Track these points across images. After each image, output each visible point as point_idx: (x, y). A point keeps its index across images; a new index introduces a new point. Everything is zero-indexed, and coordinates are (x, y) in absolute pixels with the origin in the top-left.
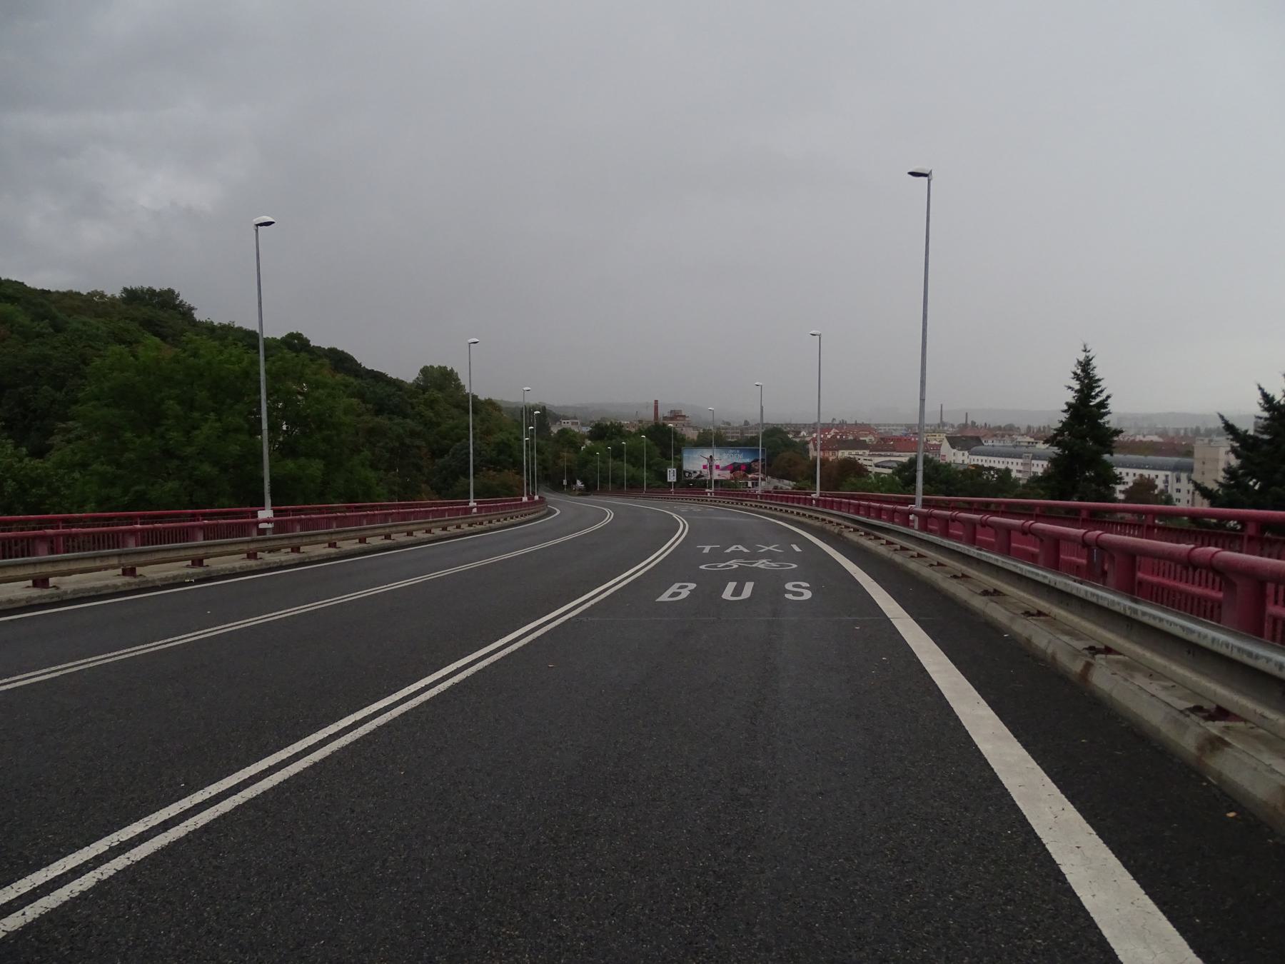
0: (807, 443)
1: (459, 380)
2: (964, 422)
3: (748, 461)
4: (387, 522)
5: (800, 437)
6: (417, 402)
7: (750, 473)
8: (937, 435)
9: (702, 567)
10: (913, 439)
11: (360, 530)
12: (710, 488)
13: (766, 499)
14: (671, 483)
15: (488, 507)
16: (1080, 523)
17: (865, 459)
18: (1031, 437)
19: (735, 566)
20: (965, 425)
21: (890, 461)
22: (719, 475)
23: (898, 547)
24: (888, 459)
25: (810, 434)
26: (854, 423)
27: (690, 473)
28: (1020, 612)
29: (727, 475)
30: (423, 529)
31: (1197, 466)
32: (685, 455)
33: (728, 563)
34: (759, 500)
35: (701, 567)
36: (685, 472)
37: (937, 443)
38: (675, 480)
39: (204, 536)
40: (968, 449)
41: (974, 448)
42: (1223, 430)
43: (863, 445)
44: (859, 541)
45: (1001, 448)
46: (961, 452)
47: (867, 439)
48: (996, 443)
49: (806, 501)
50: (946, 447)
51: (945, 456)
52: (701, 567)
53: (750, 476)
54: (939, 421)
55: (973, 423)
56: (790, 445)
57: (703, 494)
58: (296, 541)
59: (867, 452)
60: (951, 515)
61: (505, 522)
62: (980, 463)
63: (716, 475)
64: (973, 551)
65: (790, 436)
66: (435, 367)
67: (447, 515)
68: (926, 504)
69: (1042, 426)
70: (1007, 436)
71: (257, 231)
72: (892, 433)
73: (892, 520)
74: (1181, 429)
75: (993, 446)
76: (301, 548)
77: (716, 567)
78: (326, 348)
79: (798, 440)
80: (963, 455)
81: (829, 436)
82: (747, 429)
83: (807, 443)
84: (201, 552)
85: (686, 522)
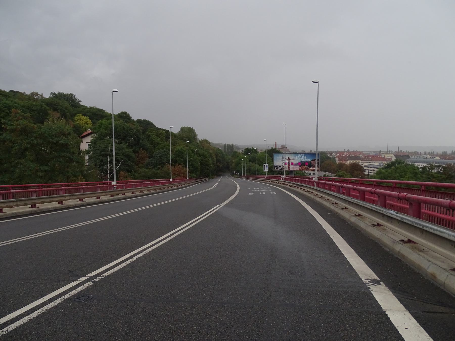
0: (335, 158)
1: (195, 132)
2: (398, 150)
5: (332, 156)
6: (152, 134)
7: (310, 167)
8: (389, 154)
10: (379, 156)
11: (148, 188)
12: (283, 175)
13: (295, 182)
14: (265, 172)
16: (374, 186)
21: (371, 165)
22: (293, 168)
23: (311, 192)
24: (370, 164)
25: (336, 154)
26: (353, 151)
27: (277, 167)
28: (370, 224)
29: (298, 168)
30: (147, 190)
36: (275, 166)
38: (268, 171)
39: (100, 190)
44: (311, 197)
45: (423, 159)
47: (360, 156)
49: (265, 178)
53: (310, 169)
54: (387, 150)
55: (401, 151)
56: (328, 158)
57: (279, 179)
58: (34, 202)
60: (324, 182)
61: (177, 187)
63: (292, 168)
64: (350, 199)
65: (328, 155)
66: (186, 127)
67: (160, 184)
69: (430, 152)
72: (370, 154)
73: (309, 184)
76: (84, 199)
78: (156, 127)
79: (331, 157)
81: (344, 155)
83: (335, 158)
84: (62, 198)
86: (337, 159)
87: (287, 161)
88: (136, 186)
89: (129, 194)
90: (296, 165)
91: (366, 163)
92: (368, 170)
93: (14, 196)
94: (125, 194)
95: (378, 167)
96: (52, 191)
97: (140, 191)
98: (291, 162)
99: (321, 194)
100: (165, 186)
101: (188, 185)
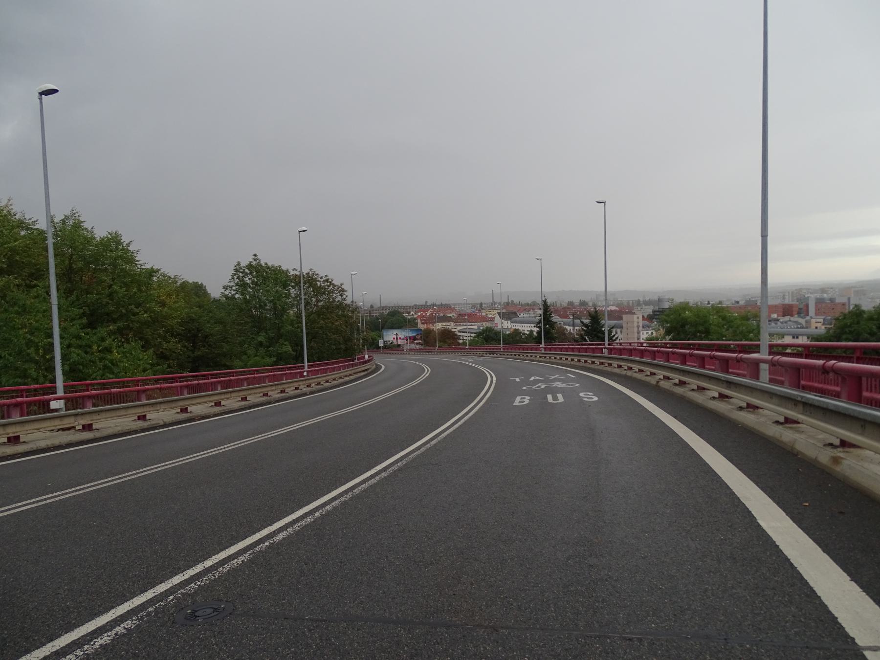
3: (414, 335)
4: (297, 378)
5: (411, 316)
7: (415, 340)
9: (524, 388)
15: (323, 369)
17: (456, 328)
18: (616, 307)
19: (543, 387)
20: (508, 304)
23: (649, 373)
24: (466, 327)
25: (416, 312)
31: (624, 325)
32: (384, 333)
33: (537, 385)
34: (543, 352)
35: (523, 388)
37: (493, 316)
40: (510, 319)
41: (514, 319)
42: (644, 299)
43: (449, 319)
46: (506, 321)
48: (525, 316)
50: (498, 319)
51: (497, 324)
52: (523, 388)
53: (415, 342)
55: (512, 301)
59: (452, 323)
62: (517, 328)
68: (309, 366)
70: (532, 310)
71: (41, 99)
74: (630, 300)
75: (524, 317)
77: (531, 388)
80: (508, 323)
81: (428, 314)
82: (373, 310)
83: (415, 319)
85: (429, 368)
86: (419, 321)
87: (395, 337)
88: (251, 382)
89: (275, 394)
90: (403, 339)
91: (460, 325)
92: (463, 336)
93: (44, 405)
94: (246, 398)
95: (475, 331)
96: (107, 397)
97: (262, 392)
98: (398, 337)
99: (695, 381)
100: (299, 383)
101: (347, 379)
